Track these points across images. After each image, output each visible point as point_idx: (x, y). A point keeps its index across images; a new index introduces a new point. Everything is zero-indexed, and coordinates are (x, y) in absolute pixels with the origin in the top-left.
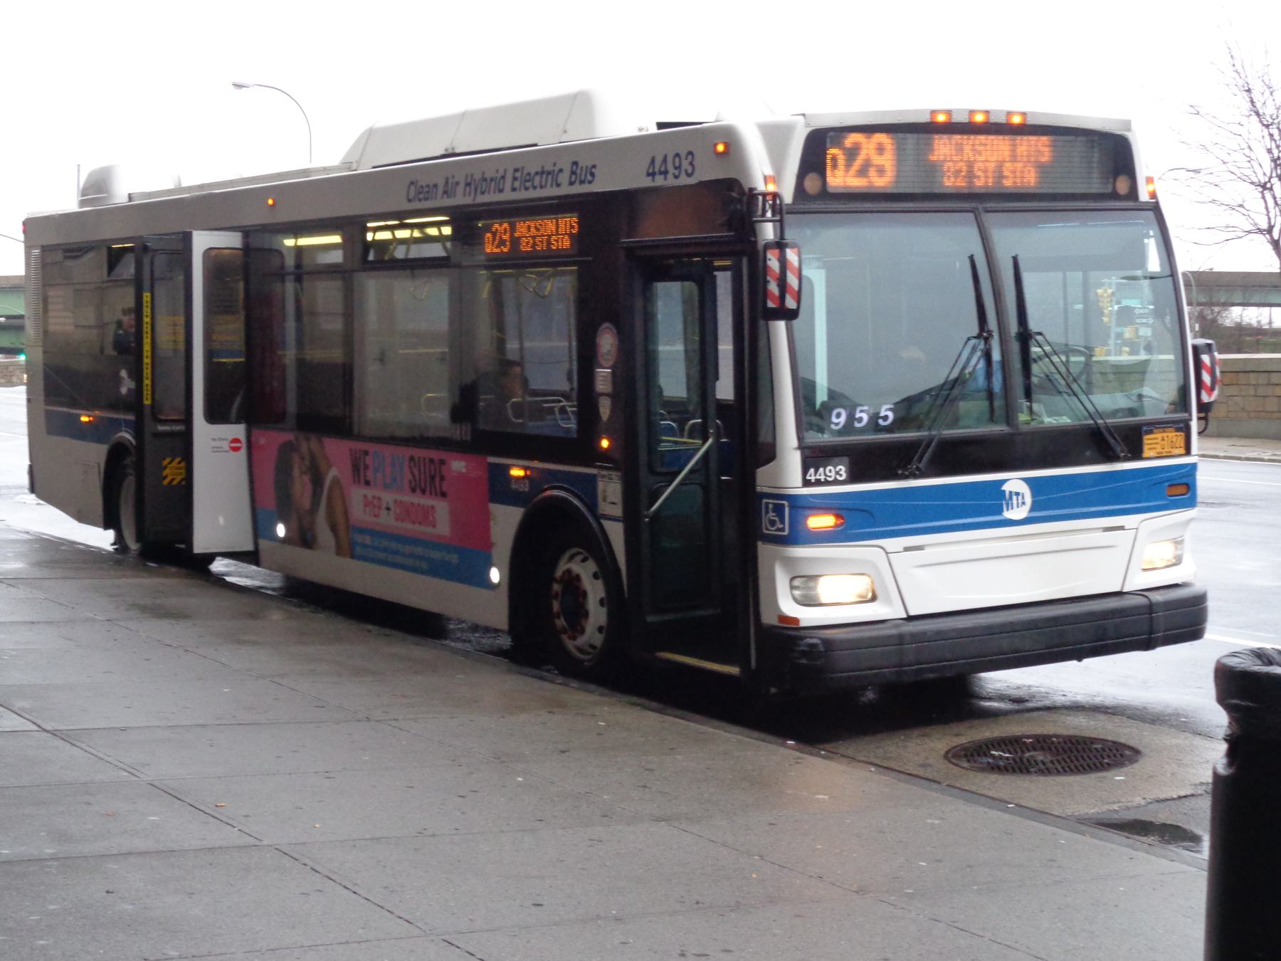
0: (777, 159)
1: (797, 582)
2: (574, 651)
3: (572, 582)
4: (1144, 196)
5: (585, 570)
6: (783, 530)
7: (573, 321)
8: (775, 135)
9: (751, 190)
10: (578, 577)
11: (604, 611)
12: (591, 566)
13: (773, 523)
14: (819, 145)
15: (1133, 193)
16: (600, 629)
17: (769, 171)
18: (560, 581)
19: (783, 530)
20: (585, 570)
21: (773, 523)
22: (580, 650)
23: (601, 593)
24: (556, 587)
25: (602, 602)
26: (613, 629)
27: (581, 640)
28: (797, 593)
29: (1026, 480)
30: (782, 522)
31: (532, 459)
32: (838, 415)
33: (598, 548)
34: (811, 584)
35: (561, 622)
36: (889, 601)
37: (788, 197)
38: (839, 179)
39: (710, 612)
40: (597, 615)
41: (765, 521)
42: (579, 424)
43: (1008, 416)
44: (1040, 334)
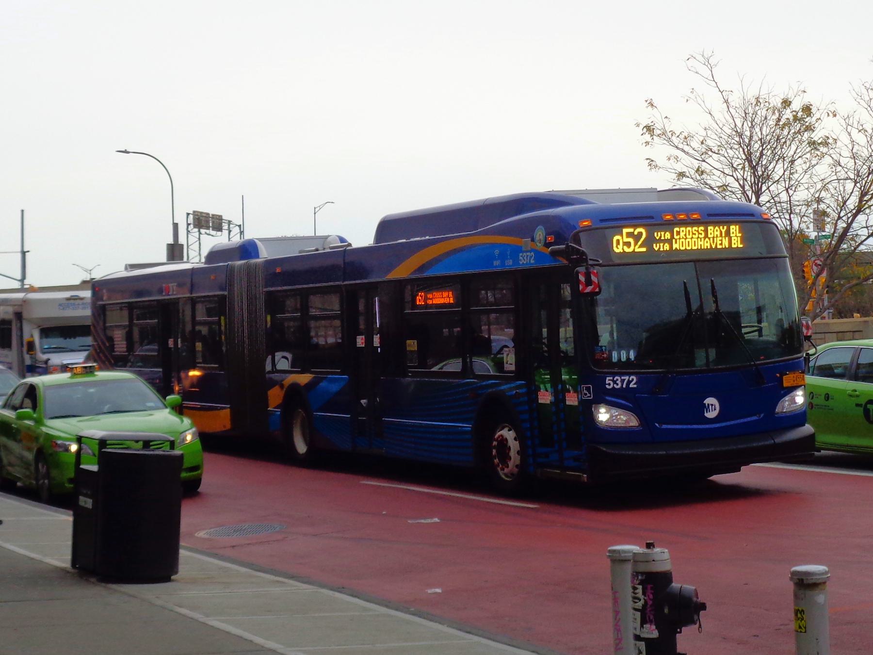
2: (503, 477)
3: (503, 441)
5: (508, 434)
7: (332, 475)
16: (517, 466)
18: (497, 440)
20: (508, 434)
22: (506, 475)
24: (495, 443)
25: (518, 453)
26: (521, 467)
27: (506, 470)
29: (580, 245)
31: (618, 332)
34: (809, 593)
35: (496, 461)
39: (754, 418)
40: (515, 458)
42: (575, 348)
43: (669, 224)
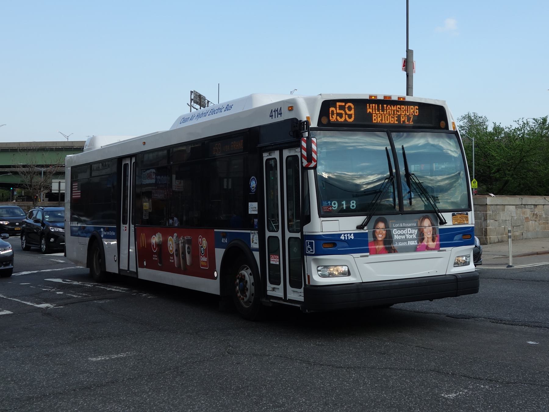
0: (311, 110)
1: (319, 268)
3: (243, 278)
4: (451, 128)
6: (313, 252)
8: (310, 101)
9: (301, 121)
10: (244, 276)
11: (252, 277)
12: (249, 271)
13: (309, 249)
14: (327, 105)
15: (447, 127)
17: (309, 114)
19: (313, 252)
21: (309, 249)
23: (252, 281)
28: (319, 272)
30: (312, 249)
32: (335, 204)
33: (251, 263)
36: (355, 276)
37: (314, 124)
38: (333, 118)
41: (307, 249)
44: (413, 174)
